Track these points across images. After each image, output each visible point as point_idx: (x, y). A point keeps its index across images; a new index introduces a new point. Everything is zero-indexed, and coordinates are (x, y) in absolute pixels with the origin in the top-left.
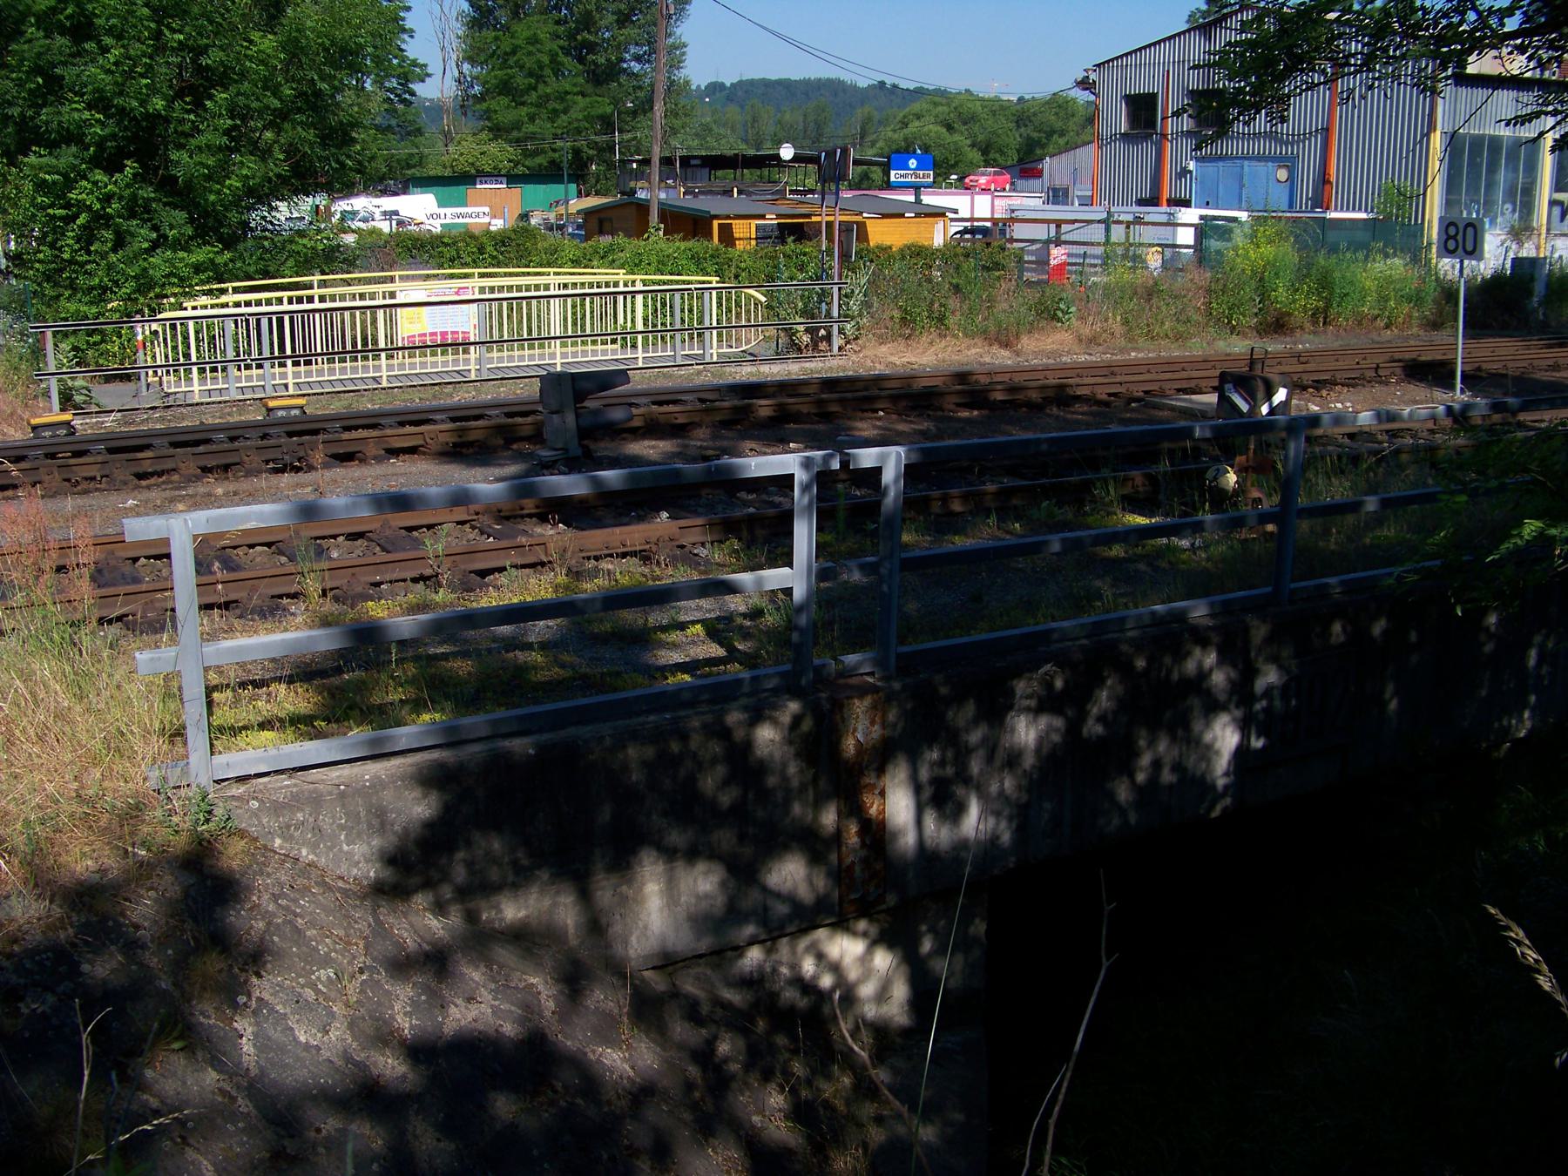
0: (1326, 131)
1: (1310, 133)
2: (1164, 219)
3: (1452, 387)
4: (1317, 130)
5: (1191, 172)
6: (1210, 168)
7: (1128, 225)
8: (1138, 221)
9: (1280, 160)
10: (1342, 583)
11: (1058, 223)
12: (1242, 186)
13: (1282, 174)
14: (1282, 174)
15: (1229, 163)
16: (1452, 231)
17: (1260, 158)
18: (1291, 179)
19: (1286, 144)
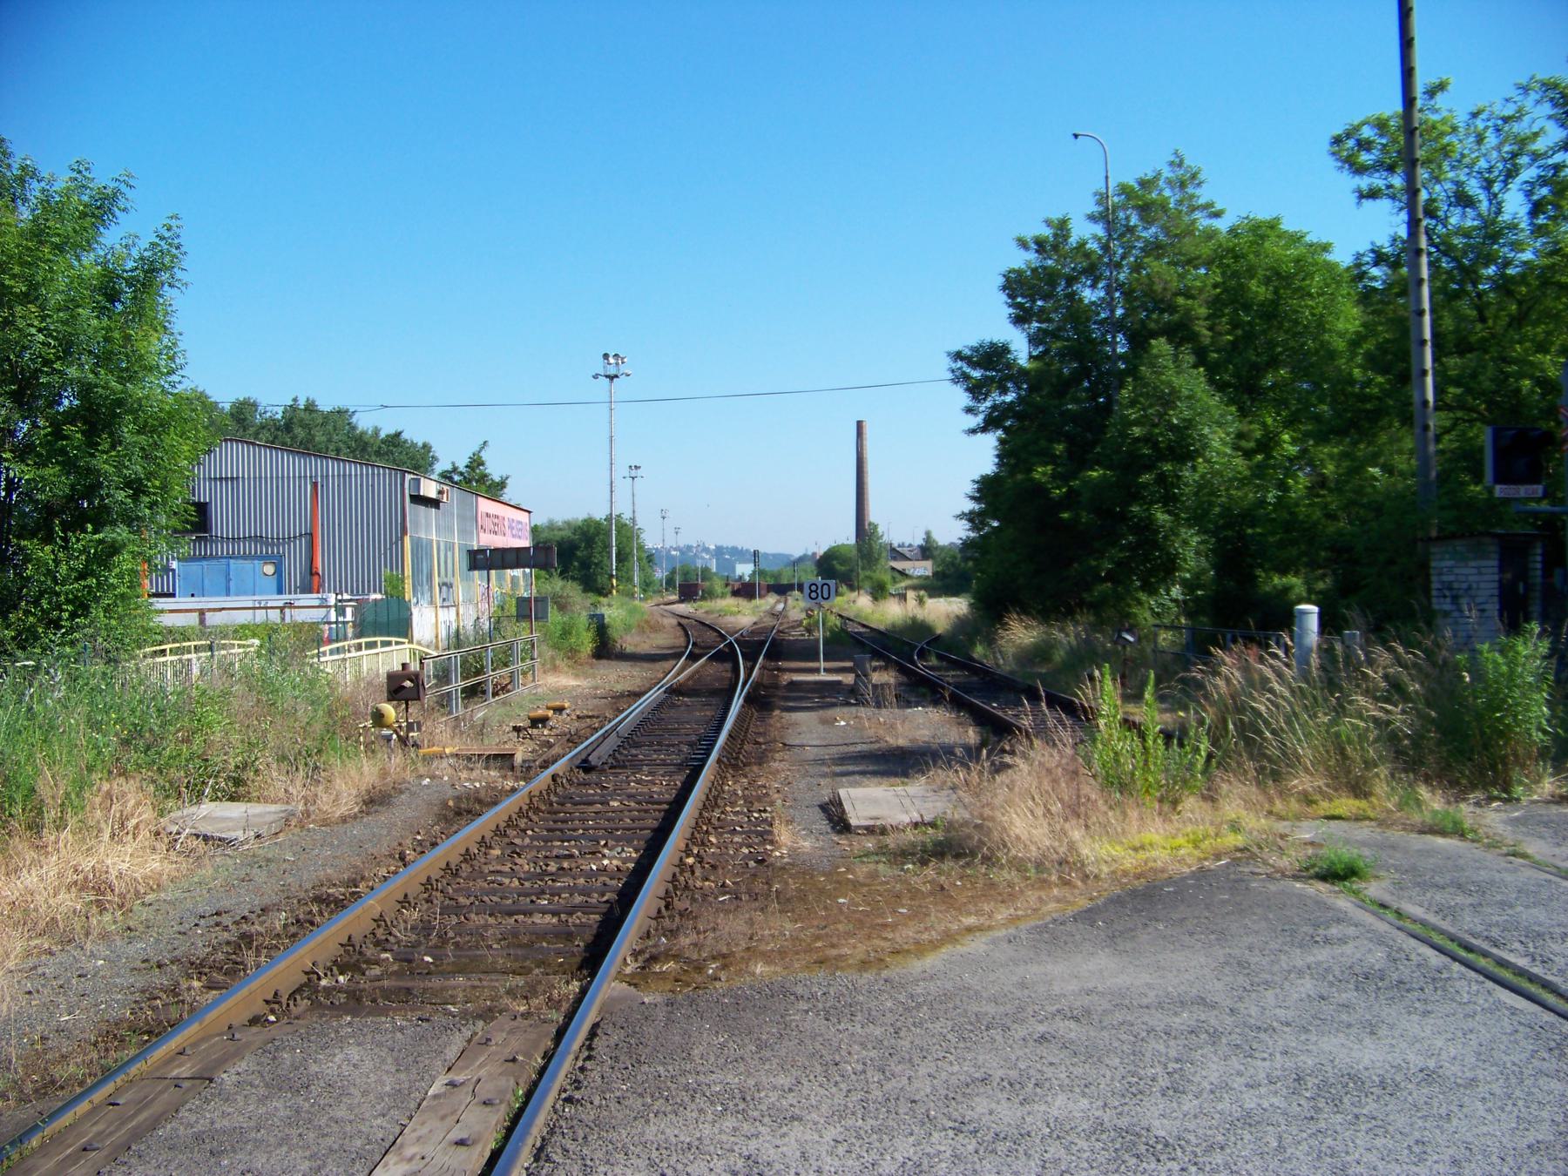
0: (311, 536)
1: (295, 537)
2: (317, 603)
3: (818, 660)
4: (301, 535)
5: (173, 570)
6: (194, 567)
7: (282, 609)
8: (290, 605)
9: (266, 559)
10: (1189, 671)
11: (202, 612)
12: (228, 580)
13: (269, 569)
14: (269, 569)
15: (214, 562)
16: (813, 588)
17: (245, 557)
18: (278, 572)
19: (273, 545)
